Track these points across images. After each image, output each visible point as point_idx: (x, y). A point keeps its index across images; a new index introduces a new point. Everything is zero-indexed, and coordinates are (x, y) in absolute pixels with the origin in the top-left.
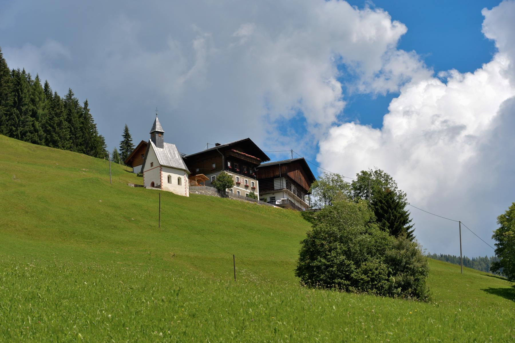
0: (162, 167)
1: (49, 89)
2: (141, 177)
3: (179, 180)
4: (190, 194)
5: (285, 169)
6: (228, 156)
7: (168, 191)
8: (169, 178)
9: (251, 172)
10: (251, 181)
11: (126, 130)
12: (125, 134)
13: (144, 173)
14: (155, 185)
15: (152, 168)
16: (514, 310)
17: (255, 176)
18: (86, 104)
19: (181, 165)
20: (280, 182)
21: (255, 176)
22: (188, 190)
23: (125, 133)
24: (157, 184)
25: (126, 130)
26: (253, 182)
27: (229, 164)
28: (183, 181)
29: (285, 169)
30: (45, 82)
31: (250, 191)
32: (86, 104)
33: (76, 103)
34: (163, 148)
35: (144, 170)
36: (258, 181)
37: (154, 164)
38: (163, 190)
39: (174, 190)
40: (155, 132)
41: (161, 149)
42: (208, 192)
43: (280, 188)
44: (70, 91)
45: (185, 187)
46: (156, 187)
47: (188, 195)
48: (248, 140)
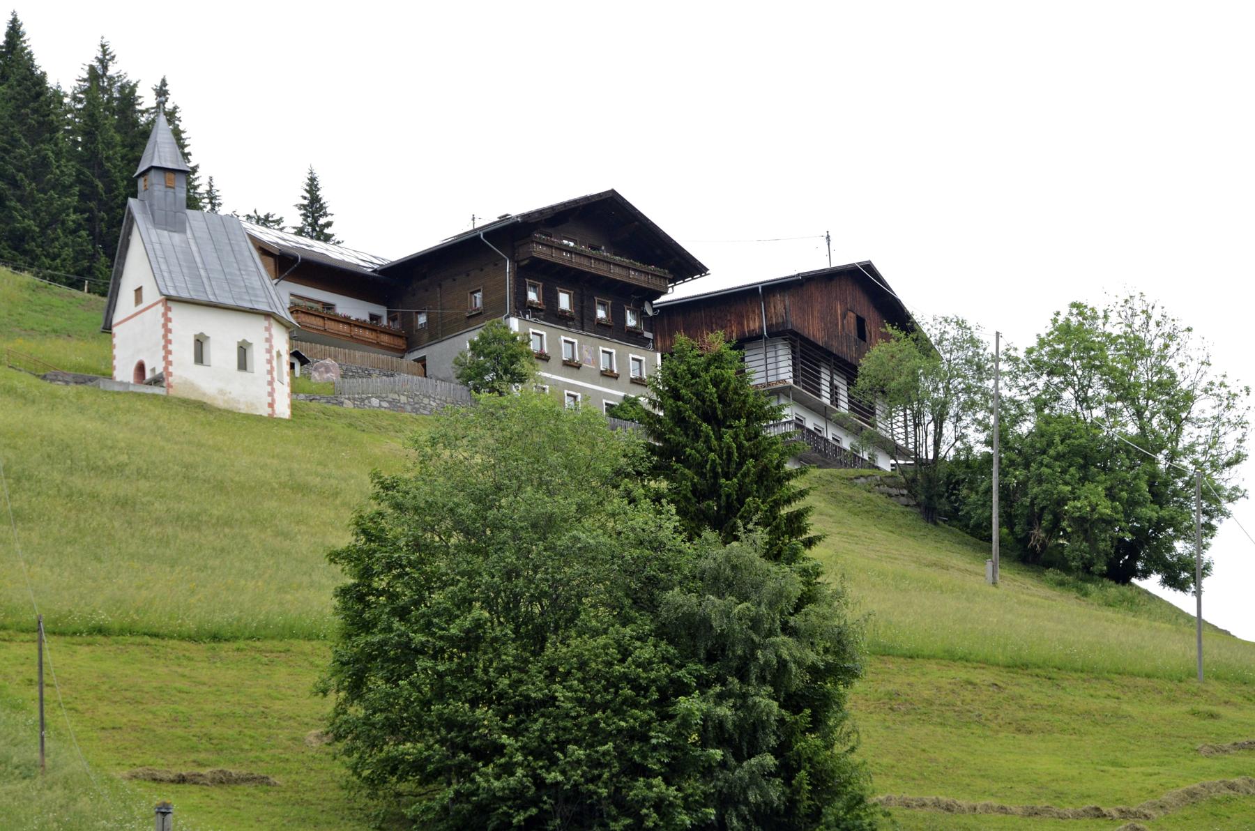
0: (170, 304)
1: (24, 42)
2: (575, 370)
3: (243, 350)
4: (293, 407)
5: (780, 306)
6: (526, 262)
7: (193, 397)
8: (200, 343)
9: (631, 321)
10: (631, 356)
11: (313, 186)
12: (306, 202)
13: (115, 330)
14: (148, 375)
15: (141, 307)
16: (722, 823)
17: (648, 335)
18: (162, 92)
19: (256, 296)
20: (762, 356)
21: (648, 335)
22: (287, 390)
23: (305, 198)
24: (153, 370)
25: (313, 186)
26: (636, 357)
27: (532, 296)
28: (258, 357)
29: (780, 306)
30: (11, 18)
31: (622, 394)
32: (162, 92)
33: (128, 96)
34: (184, 231)
35: (117, 318)
36: (659, 355)
37: (145, 292)
38: (172, 392)
39: (222, 392)
40: (153, 172)
41: (177, 237)
42: (426, 401)
43: (763, 381)
44: (103, 46)
45: (269, 378)
46: (149, 383)
47: (283, 409)
48: (612, 198)
